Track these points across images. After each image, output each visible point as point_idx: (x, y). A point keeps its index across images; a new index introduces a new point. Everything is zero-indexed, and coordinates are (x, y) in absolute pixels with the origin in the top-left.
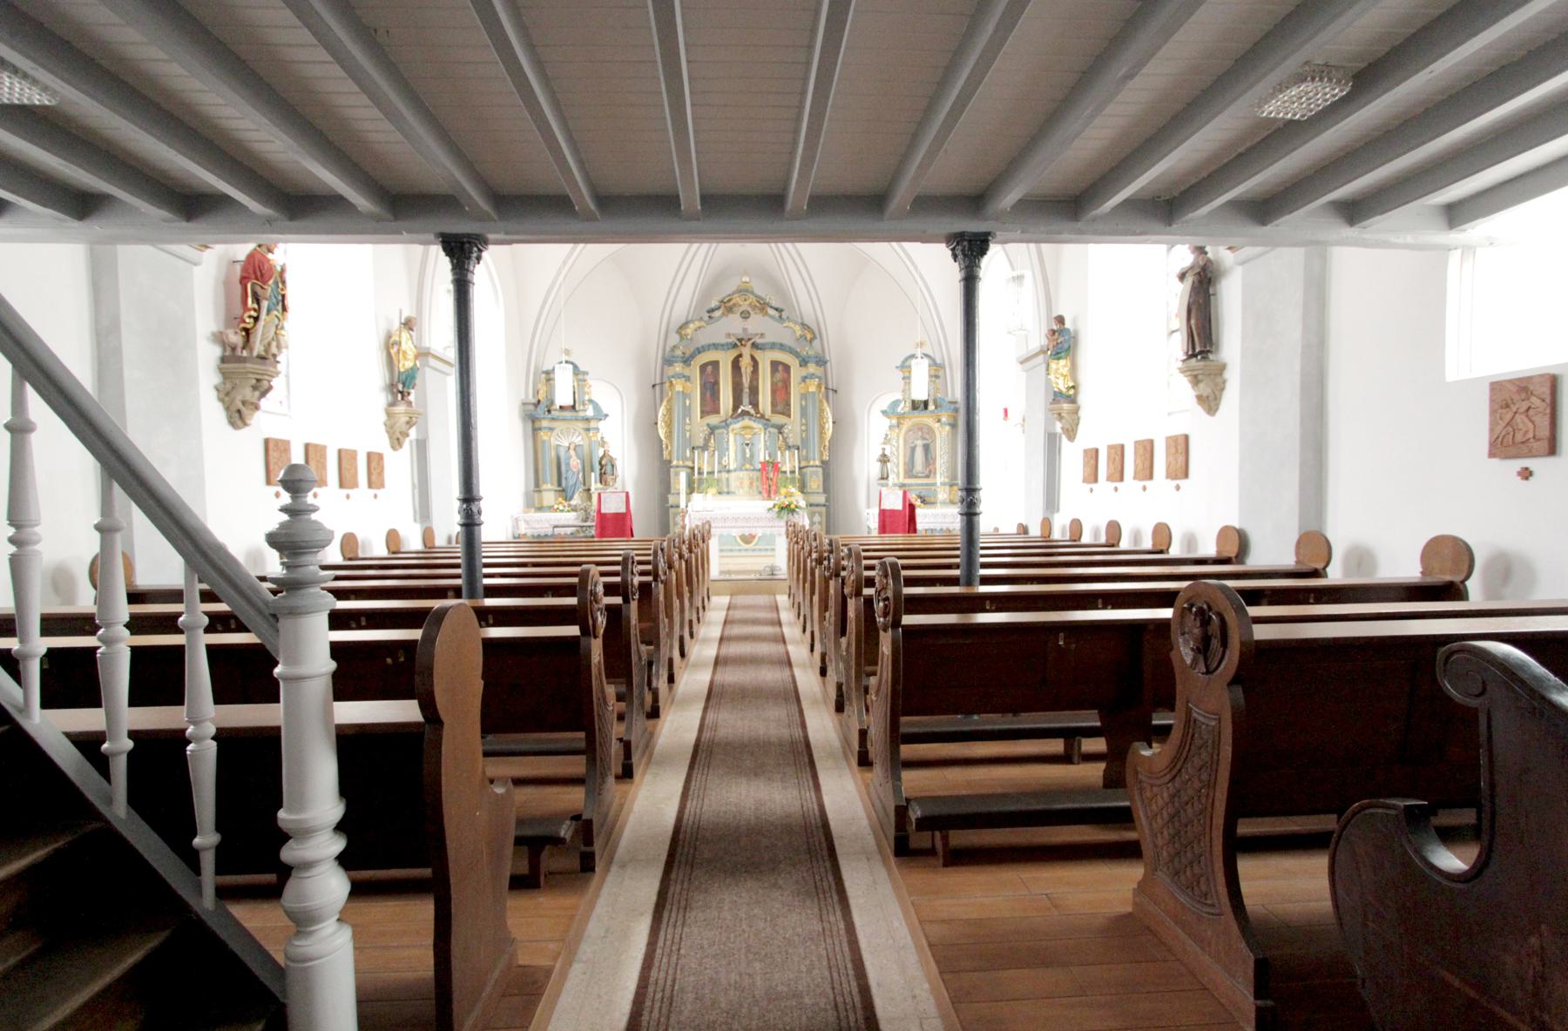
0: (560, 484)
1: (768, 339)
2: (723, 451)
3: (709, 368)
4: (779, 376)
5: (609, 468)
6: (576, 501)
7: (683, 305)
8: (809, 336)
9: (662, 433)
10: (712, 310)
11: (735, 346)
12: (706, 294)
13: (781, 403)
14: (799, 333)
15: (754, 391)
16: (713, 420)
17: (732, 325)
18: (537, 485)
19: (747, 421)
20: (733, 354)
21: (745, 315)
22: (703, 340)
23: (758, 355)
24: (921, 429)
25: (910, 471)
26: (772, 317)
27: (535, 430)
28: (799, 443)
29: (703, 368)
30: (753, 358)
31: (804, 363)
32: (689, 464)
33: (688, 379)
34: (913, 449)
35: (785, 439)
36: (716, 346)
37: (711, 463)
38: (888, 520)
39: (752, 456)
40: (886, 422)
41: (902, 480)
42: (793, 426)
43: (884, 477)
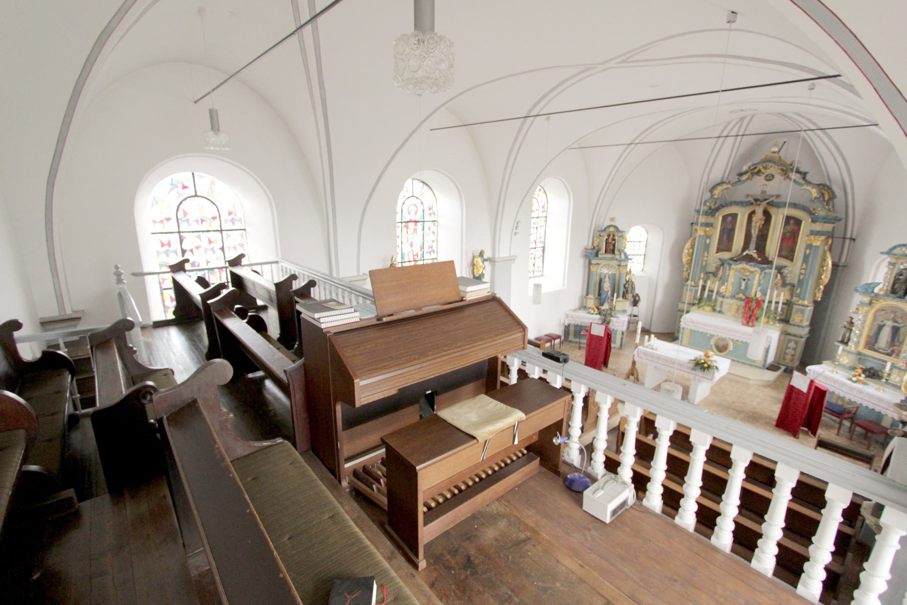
0: (599, 294)
2: (723, 281)
3: (729, 219)
6: (606, 306)
7: (718, 173)
9: (685, 259)
10: (741, 174)
11: (752, 204)
13: (788, 249)
16: (726, 255)
17: (757, 186)
18: (587, 295)
20: (748, 210)
24: (892, 312)
25: (871, 343)
27: (590, 263)
28: (795, 282)
29: (725, 218)
34: (881, 327)
38: (794, 396)
39: (747, 287)
41: (861, 348)
42: (794, 269)
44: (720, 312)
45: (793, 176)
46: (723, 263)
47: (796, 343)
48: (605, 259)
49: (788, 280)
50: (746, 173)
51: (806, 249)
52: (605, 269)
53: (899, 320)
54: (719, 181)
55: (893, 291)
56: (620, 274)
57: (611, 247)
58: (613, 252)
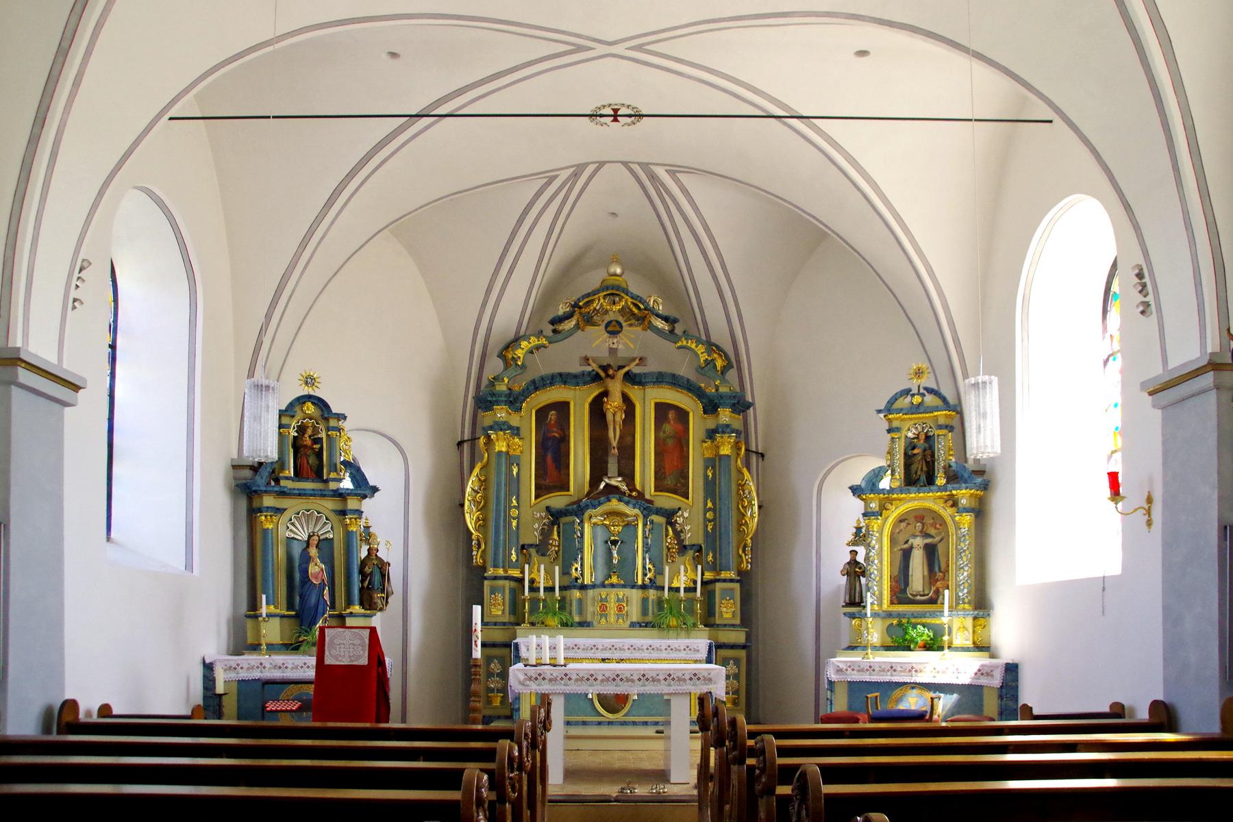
1: (652, 367)
3: (552, 415)
4: (668, 428)
5: (377, 578)
8: (719, 363)
12: (550, 294)
13: (672, 475)
14: (704, 358)
15: (627, 452)
16: (558, 501)
17: (596, 343)
19: (615, 504)
20: (594, 391)
21: (614, 329)
22: (543, 366)
23: (635, 393)
25: (900, 593)
26: (659, 332)
27: (253, 512)
28: (700, 540)
29: (542, 413)
30: (626, 398)
31: (711, 407)
32: (515, 573)
33: (516, 432)
34: (907, 554)
35: (677, 534)
36: (565, 379)
37: (550, 574)
40: (857, 506)
43: (855, 601)
44: (584, 624)
45: (660, 324)
46: (556, 516)
47: (737, 661)
48: (301, 494)
49: (688, 538)
50: (568, 316)
51: (706, 468)
52: (294, 525)
53: (932, 531)
54: (511, 336)
55: (910, 481)
56: (348, 535)
57: (312, 460)
58: (318, 475)
